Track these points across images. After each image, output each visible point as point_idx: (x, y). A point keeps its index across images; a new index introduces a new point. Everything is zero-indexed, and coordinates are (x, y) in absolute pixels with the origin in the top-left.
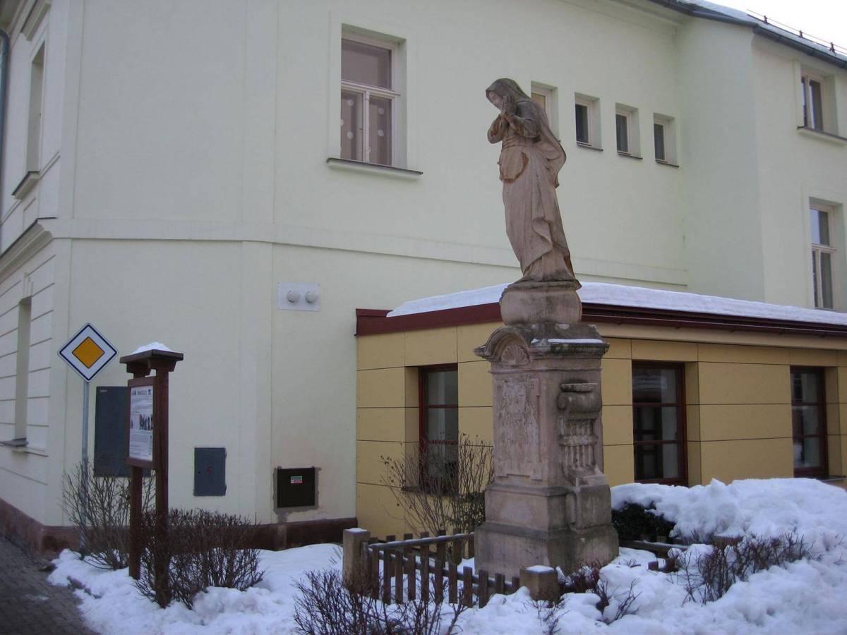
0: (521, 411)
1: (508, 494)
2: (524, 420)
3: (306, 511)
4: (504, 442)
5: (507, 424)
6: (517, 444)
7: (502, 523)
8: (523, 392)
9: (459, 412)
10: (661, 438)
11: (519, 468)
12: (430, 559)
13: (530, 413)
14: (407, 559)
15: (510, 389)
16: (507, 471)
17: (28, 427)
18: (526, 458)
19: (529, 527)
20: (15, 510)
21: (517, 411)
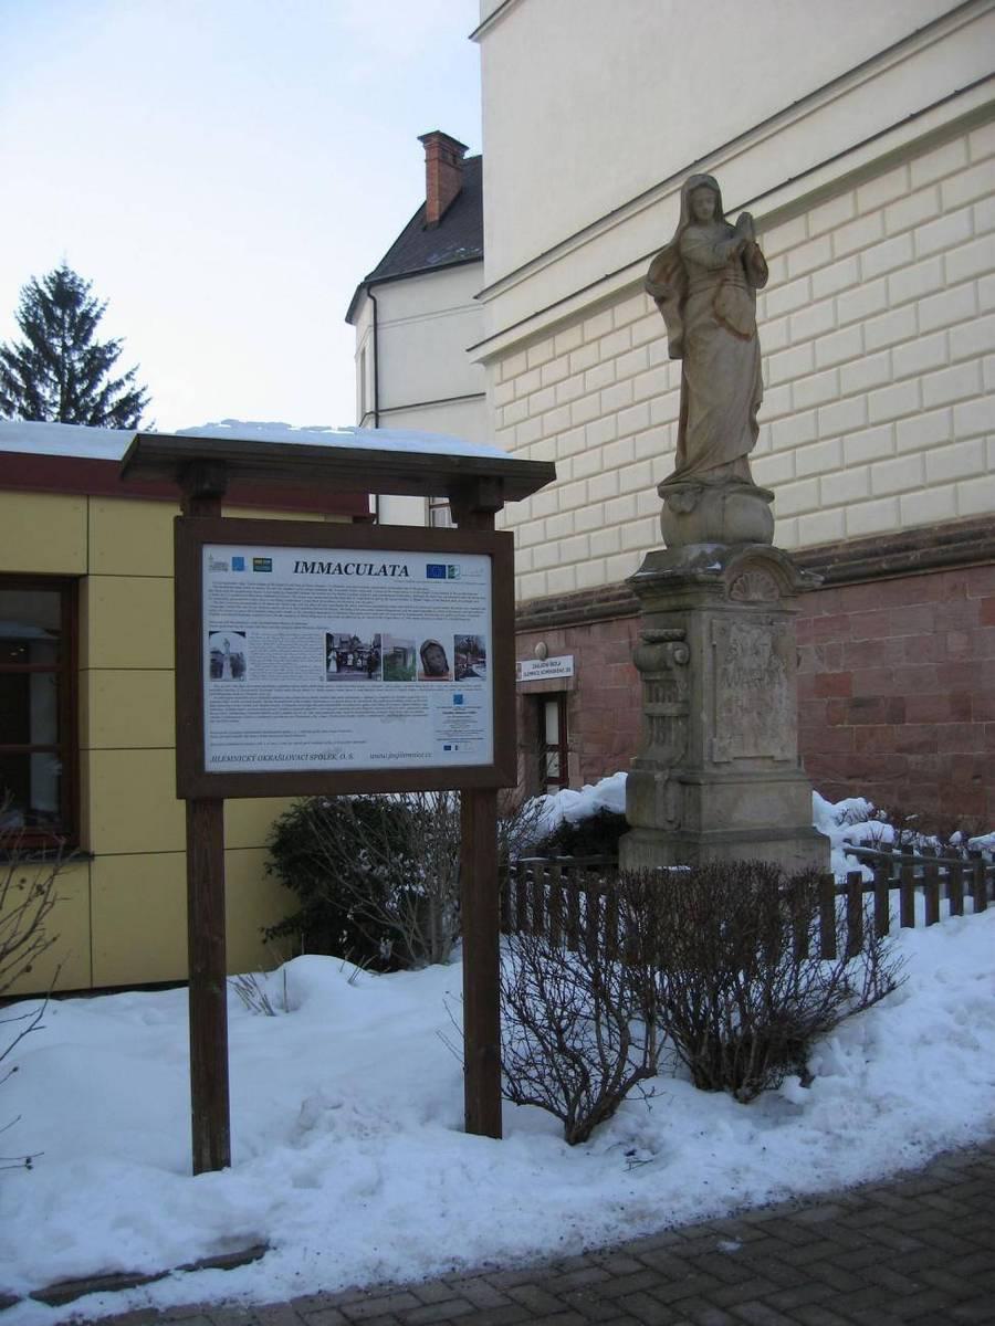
0: (763, 667)
1: (746, 786)
2: (767, 679)
3: (93, 997)
4: (730, 710)
5: (736, 684)
6: (755, 714)
7: (731, 829)
8: (767, 639)
9: (90, 677)
10: (27, 740)
11: (756, 745)
12: (891, 892)
13: (777, 669)
14: (723, 926)
15: (744, 634)
16: (734, 752)
17: (184, 975)
18: (770, 732)
19: (783, 826)
20: (778, 225)
21: (755, 666)
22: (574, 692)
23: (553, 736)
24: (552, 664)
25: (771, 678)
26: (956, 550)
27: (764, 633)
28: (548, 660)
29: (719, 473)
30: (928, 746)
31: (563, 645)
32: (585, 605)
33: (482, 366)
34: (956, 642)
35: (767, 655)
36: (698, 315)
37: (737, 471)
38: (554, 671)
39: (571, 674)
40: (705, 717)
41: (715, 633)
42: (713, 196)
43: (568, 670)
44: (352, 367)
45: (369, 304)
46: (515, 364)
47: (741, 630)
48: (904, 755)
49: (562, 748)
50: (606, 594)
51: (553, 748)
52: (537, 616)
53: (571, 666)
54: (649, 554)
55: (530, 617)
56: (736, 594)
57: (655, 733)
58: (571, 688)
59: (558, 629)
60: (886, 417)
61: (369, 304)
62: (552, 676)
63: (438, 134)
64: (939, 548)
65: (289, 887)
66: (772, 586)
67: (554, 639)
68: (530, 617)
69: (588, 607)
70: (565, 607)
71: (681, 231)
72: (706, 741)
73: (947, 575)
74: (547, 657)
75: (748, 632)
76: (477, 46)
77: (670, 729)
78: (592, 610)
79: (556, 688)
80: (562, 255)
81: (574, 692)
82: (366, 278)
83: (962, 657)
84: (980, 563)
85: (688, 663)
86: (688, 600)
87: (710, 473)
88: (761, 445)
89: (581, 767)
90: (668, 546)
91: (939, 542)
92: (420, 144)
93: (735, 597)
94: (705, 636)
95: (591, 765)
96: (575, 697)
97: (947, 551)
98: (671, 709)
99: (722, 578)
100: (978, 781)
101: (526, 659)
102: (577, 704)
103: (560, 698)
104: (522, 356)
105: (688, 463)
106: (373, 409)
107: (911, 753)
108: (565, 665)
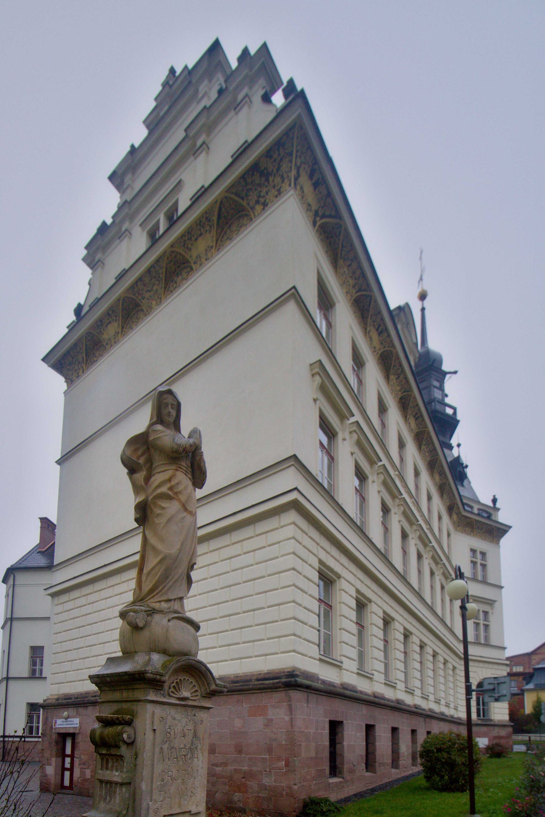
0: (188, 746)
8: (191, 726)
11: (180, 806)
21: (182, 746)
22: (79, 733)
23: (68, 751)
24: (70, 721)
25: (193, 754)
26: (240, 686)
27: (190, 721)
28: (69, 720)
29: (164, 605)
30: (225, 764)
31: (75, 713)
32: (86, 698)
33: (50, 598)
34: (238, 723)
35: (191, 738)
36: (159, 486)
37: (176, 606)
38: (71, 724)
39: (78, 726)
40: (144, 786)
41: (156, 720)
42: (175, 403)
43: (77, 724)
44: (4, 600)
45: (12, 576)
46: (64, 598)
47: (174, 719)
48: (214, 767)
49: (72, 756)
50: (95, 694)
51: (68, 756)
52: (66, 701)
53: (78, 722)
54: (108, 659)
55: (62, 701)
56: (173, 692)
57: (104, 793)
58: (77, 731)
59: (74, 707)
60: (262, 591)
61: (12, 576)
62: (69, 726)
63: (46, 519)
64: (233, 685)
65: (163, 685)
66: (197, 688)
67: (71, 711)
68: (62, 701)
69: (87, 699)
70: (77, 698)
71: (151, 425)
72: (144, 805)
73: (235, 696)
74: (68, 718)
75: (179, 721)
76: (59, 467)
77: (115, 792)
78: (89, 700)
79: (71, 731)
80: (88, 555)
81: (79, 733)
82: (11, 566)
83: (240, 729)
84: (250, 692)
85: (133, 742)
86: (352, 301)
87: (158, 604)
88: (192, 591)
89: (80, 764)
90: (123, 654)
91: (234, 682)
92: (39, 520)
93: (171, 694)
94: (148, 722)
95: (84, 764)
96: (79, 736)
97: (237, 686)
98: (116, 776)
99: (163, 679)
100: (244, 780)
101: (59, 719)
102: (79, 739)
103: (73, 736)
104: (67, 594)
105: (142, 595)
106: (10, 617)
107: (217, 767)
108: (76, 722)
